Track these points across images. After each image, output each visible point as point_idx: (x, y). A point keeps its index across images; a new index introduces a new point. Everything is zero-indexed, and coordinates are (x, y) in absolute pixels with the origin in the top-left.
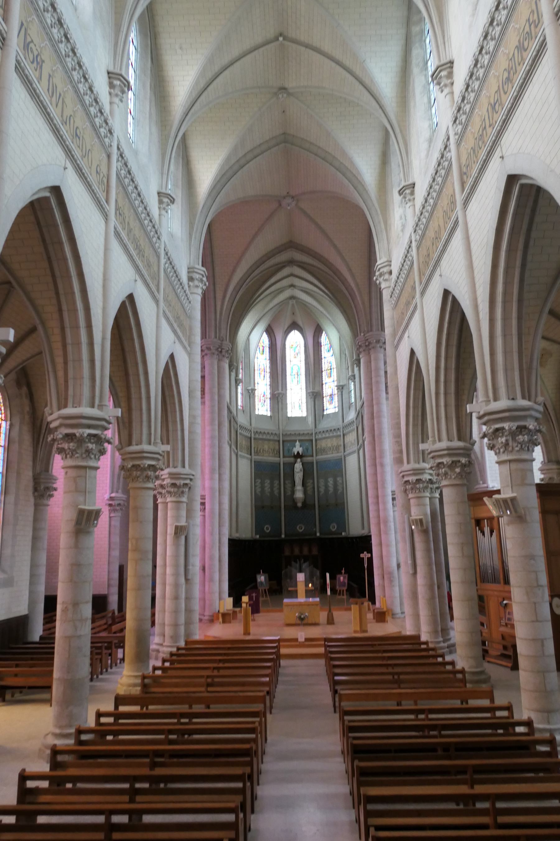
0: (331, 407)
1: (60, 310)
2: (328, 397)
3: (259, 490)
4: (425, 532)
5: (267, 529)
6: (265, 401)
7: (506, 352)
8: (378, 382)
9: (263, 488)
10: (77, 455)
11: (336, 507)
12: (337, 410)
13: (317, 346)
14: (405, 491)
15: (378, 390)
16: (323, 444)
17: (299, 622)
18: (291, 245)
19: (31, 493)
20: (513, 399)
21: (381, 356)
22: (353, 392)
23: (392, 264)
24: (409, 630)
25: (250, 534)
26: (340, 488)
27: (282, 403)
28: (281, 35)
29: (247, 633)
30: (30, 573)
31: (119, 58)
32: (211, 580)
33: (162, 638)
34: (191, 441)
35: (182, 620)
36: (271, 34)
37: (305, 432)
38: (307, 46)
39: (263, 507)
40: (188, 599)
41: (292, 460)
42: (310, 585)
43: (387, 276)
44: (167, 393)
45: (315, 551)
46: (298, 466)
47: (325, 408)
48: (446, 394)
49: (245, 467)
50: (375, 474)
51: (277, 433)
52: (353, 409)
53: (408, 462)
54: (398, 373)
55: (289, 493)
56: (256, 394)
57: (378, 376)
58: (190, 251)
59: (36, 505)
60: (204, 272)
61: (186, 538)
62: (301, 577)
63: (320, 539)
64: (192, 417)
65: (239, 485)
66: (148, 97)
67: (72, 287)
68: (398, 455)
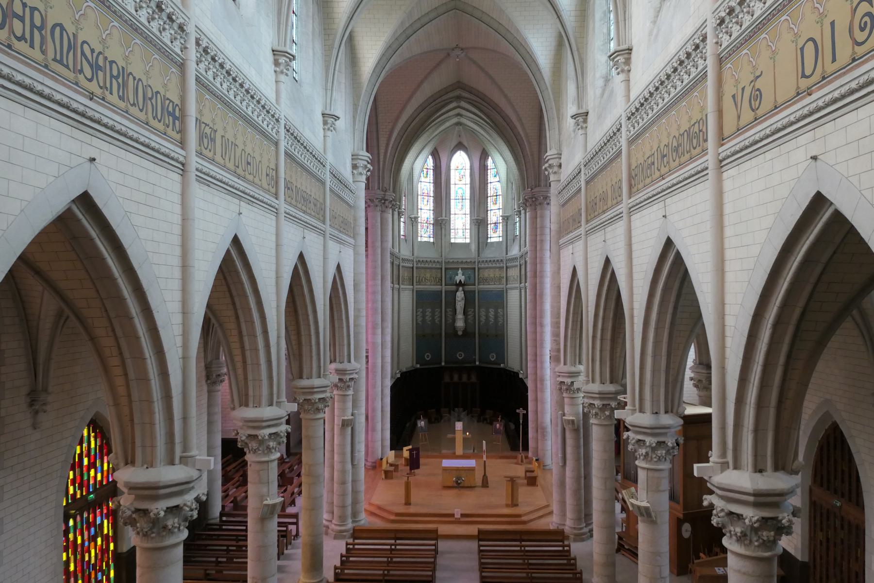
0: (495, 236)
1: (237, 317)
3: (420, 319)
4: (576, 431)
5: (428, 356)
7: (654, 371)
9: (424, 316)
11: (496, 337)
12: (501, 239)
13: (484, 169)
14: (560, 389)
15: (542, 249)
16: (486, 274)
18: (460, 85)
19: (204, 382)
23: (562, 157)
26: (500, 319)
29: (408, 503)
31: (283, 27)
32: (374, 430)
34: (357, 334)
35: (349, 500)
39: (424, 336)
43: (556, 169)
44: (334, 302)
45: (474, 379)
46: (460, 295)
48: (602, 340)
49: (407, 298)
50: (535, 332)
51: (440, 260)
52: (517, 242)
53: (565, 364)
54: (562, 272)
57: (542, 234)
58: (354, 128)
61: (352, 429)
63: (478, 367)
64: (357, 310)
65: (401, 319)
66: (311, 14)
67: (248, 303)
68: (555, 354)
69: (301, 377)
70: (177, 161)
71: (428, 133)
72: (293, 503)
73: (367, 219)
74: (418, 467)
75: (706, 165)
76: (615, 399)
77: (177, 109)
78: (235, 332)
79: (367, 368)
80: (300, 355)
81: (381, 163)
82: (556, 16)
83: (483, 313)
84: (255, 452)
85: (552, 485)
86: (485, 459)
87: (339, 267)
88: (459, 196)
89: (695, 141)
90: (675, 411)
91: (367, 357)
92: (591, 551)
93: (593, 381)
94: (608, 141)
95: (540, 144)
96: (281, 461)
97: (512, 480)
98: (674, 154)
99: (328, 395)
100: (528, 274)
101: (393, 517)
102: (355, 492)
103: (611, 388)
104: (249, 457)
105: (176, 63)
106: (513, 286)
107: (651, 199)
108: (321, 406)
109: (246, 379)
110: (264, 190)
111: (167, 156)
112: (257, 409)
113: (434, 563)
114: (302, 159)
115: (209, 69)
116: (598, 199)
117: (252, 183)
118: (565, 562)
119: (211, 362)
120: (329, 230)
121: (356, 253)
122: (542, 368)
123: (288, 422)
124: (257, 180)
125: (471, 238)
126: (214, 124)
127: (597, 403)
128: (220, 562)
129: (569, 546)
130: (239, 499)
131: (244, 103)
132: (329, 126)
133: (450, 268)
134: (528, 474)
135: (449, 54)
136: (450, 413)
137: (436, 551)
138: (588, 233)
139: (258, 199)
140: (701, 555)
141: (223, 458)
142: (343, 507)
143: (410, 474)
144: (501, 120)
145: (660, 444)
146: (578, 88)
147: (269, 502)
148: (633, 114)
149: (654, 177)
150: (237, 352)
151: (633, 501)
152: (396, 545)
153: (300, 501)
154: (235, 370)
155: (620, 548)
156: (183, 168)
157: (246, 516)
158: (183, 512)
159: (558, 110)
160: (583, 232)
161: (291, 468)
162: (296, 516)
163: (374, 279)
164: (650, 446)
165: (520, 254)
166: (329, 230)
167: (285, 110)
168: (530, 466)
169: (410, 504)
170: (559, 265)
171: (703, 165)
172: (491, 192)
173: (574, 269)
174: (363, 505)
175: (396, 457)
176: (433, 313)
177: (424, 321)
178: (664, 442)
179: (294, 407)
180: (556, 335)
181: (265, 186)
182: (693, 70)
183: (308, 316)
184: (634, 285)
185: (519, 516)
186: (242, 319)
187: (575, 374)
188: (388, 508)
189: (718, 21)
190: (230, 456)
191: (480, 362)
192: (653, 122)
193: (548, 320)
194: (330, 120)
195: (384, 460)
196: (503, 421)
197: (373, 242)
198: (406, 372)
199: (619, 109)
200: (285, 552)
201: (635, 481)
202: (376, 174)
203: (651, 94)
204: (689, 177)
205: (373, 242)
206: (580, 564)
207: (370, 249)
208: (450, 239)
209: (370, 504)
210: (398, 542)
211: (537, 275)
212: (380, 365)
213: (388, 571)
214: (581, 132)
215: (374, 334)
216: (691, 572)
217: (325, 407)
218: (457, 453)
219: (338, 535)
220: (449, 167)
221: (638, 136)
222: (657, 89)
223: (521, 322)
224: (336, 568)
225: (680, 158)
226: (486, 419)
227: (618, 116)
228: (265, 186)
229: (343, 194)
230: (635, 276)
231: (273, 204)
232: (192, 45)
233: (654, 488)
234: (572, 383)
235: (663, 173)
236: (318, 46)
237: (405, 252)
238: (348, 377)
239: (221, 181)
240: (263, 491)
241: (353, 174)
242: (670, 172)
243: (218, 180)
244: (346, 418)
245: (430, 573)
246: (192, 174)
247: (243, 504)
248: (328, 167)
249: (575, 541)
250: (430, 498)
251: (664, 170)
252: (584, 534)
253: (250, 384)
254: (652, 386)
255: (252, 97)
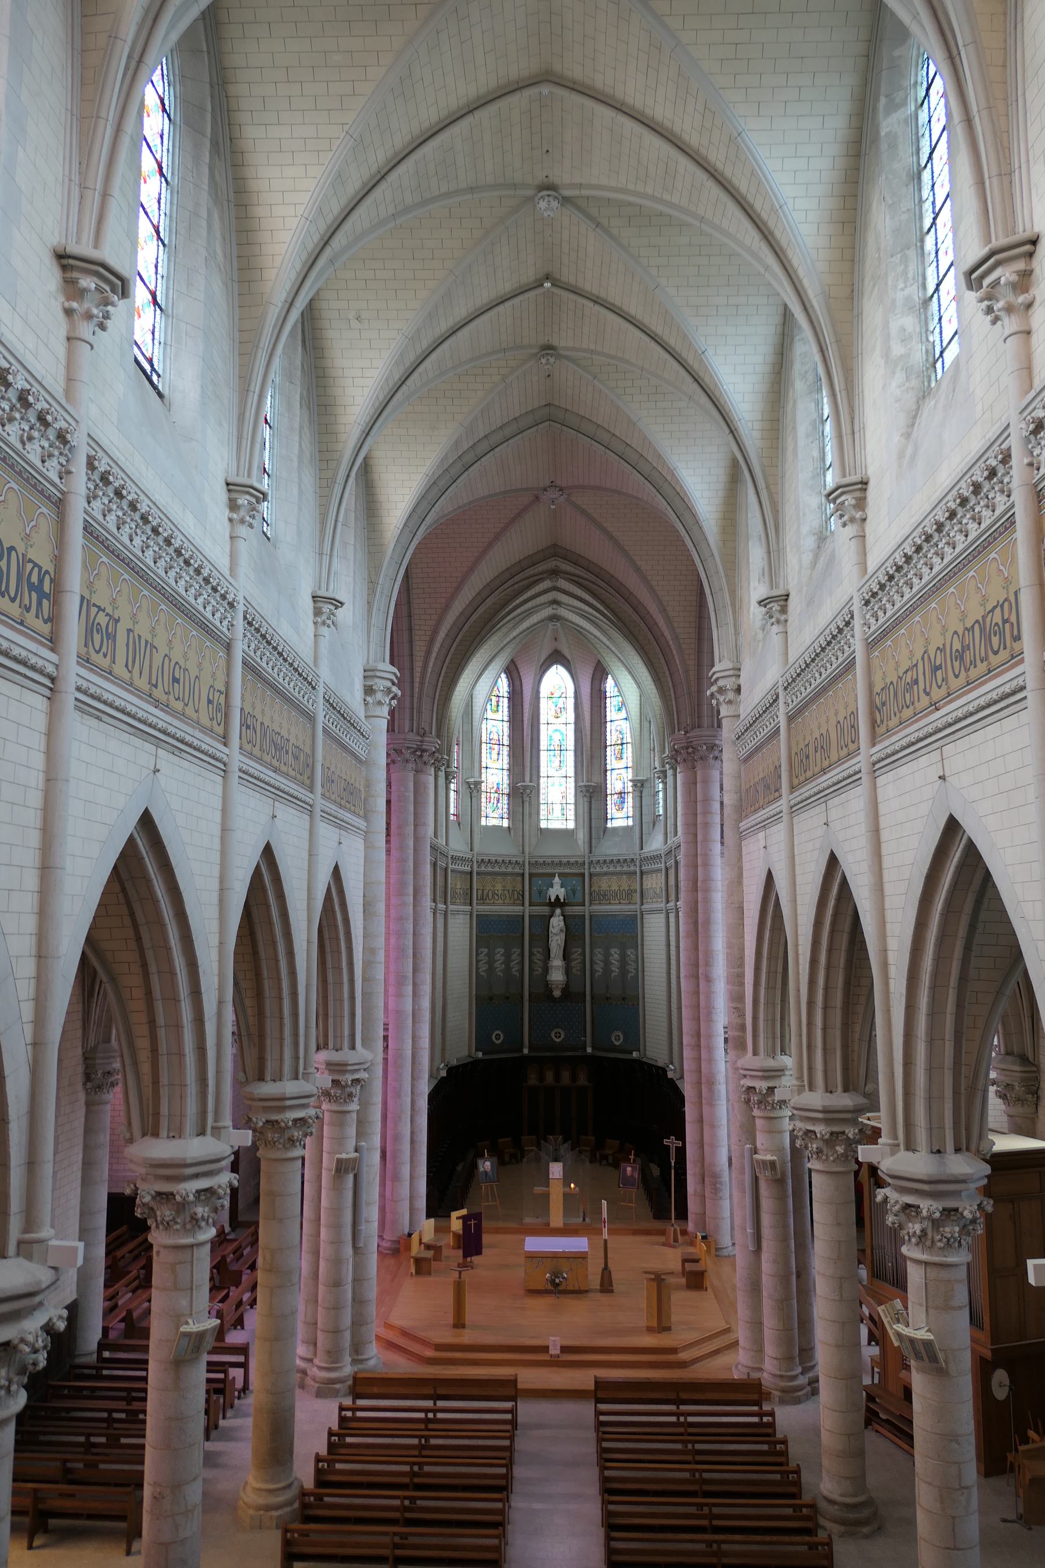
1: (144, 965)
2: (616, 796)
3: (484, 967)
4: (780, 1182)
5: (498, 1037)
6: (498, 802)
7: (931, 1070)
8: (707, 825)
9: (491, 963)
10: (178, 1227)
11: (622, 1002)
12: (630, 822)
13: (599, 698)
14: (748, 1101)
15: (706, 840)
16: (604, 884)
17: (550, 1287)
18: (555, 551)
19: (79, 1086)
20: (939, 1152)
21: (715, 774)
22: (661, 794)
23: (742, 674)
24: (746, 1355)
25: (466, 1048)
26: (631, 968)
27: (530, 804)
28: (547, 277)
29: (459, 1324)
30: (81, 1210)
31: (246, 444)
33: (311, 1348)
34: (367, 995)
36: (529, 275)
37: (572, 860)
38: (597, 301)
40: (358, 1280)
41: (546, 910)
42: (572, 1185)
43: (731, 695)
44: (326, 936)
45: (582, 1080)
46: (557, 923)
47: (609, 816)
48: (826, 1008)
49: (460, 929)
50: (697, 993)
51: (520, 860)
52: (660, 827)
53: (755, 1053)
54: (745, 881)
55: (539, 971)
56: (483, 788)
57: (707, 812)
58: (369, 636)
59: (89, 1104)
60: (395, 674)
61: (356, 1177)
62: (556, 1170)
63: (592, 1057)
64: (369, 951)
66: (296, 425)
69: (261, 1078)
70: (41, 672)
71: (500, 634)
72: (239, 1323)
73: (389, 785)
74: (479, 1252)
75: (1020, 681)
76: (854, 1122)
77: (47, 579)
78: (138, 993)
79: (386, 1060)
80: (262, 1036)
81: (417, 685)
82: (727, 431)
83: (599, 956)
84: (168, 1226)
85: (740, 1298)
86: (605, 1235)
87: (336, 872)
88: (555, 748)
89: (995, 640)
90: (973, 1147)
91: (386, 1038)
92: (816, 1424)
93: (812, 1087)
94: (829, 643)
95: (699, 652)
96: (220, 1241)
97: (658, 1279)
98: (957, 664)
99: (312, 1112)
100: (682, 885)
101: (430, 1353)
102: (359, 1301)
103: (844, 1100)
104: (157, 1237)
105: (49, 498)
106: (654, 906)
107: (914, 747)
108: (297, 1134)
109: (156, 1082)
110: (204, 729)
111: (24, 663)
112: (176, 1142)
113: (510, 1449)
114: (274, 673)
115: (148, 547)
116: (811, 748)
117: (182, 716)
118: (765, 1447)
119: (94, 1049)
120: (320, 803)
121: (368, 847)
122: (711, 1060)
123: (235, 1168)
124: (190, 711)
125: (576, 820)
126: (115, 608)
127: (820, 1129)
128: (95, 1445)
129: (772, 1414)
130: (135, 1315)
131: (172, 574)
132: (324, 617)
133: (538, 874)
134: (689, 1267)
135: (537, 498)
136: (539, 1146)
137: (514, 1423)
138: (794, 810)
139: (190, 746)
140: (1031, 1434)
141: (110, 1229)
142: (335, 1332)
143: (464, 1265)
144: (630, 610)
145: (949, 1213)
146: (769, 552)
147: (192, 1327)
148: (874, 595)
149: (919, 706)
150: (141, 1030)
151: (900, 1328)
152: (435, 1411)
153: (254, 1319)
154: (135, 1063)
155: (871, 1418)
156: (53, 685)
157: (145, 1349)
158: (18, 1355)
159: (733, 592)
160: (785, 809)
161: (238, 1253)
162: (243, 1350)
163: (401, 893)
164: (930, 1218)
165: (666, 848)
166: (320, 803)
167: (245, 587)
168: (691, 1250)
169: (463, 1326)
170: (741, 868)
171: (1014, 683)
172: (612, 738)
173: (770, 876)
174: (374, 1328)
175: (437, 1230)
176: (508, 956)
177: (491, 968)
178: (956, 1210)
179: (245, 1138)
180: (737, 998)
181: (205, 720)
182: (986, 513)
183: (277, 961)
184: (887, 905)
185: (674, 1351)
186: (153, 968)
187: (776, 1073)
188: (422, 1334)
189: (1032, 427)
190: (124, 1228)
191: (593, 1048)
192: (913, 609)
193: (720, 970)
194: (326, 608)
195: (415, 1237)
196: (639, 1160)
197: (400, 827)
198: (457, 1067)
199: (846, 587)
200: (222, 1423)
201: (900, 1283)
202: (407, 704)
203: (908, 559)
204: (989, 705)
205: (400, 827)
206: (795, 1451)
207: (392, 838)
208: (538, 820)
209: (388, 1326)
210: (441, 1404)
211: (699, 886)
212: (409, 1053)
213: (421, 1465)
214: (775, 629)
215: (399, 995)
216: (1012, 1470)
217: (306, 1135)
218: (553, 1225)
219: (325, 1390)
220: (538, 692)
221: (885, 634)
222: (919, 549)
223: (669, 973)
224: (318, 1459)
225: (967, 670)
226: (605, 1157)
227: (846, 598)
228: (205, 720)
229: (346, 740)
230: (888, 889)
231: (218, 754)
232: (80, 467)
233: (938, 1303)
234: (771, 1090)
235: (935, 698)
236: (309, 480)
237: (457, 845)
238: (350, 1077)
239: (123, 711)
240: (181, 1305)
241: (366, 704)
242: (950, 696)
243: (117, 709)
244: (344, 1156)
245: (503, 1470)
246: (69, 696)
247: (143, 1324)
248: (321, 690)
249: (783, 1402)
250: (509, 1317)
251: (937, 694)
252: (800, 1388)
253: (164, 1092)
254: (929, 1099)
255: (187, 563)
